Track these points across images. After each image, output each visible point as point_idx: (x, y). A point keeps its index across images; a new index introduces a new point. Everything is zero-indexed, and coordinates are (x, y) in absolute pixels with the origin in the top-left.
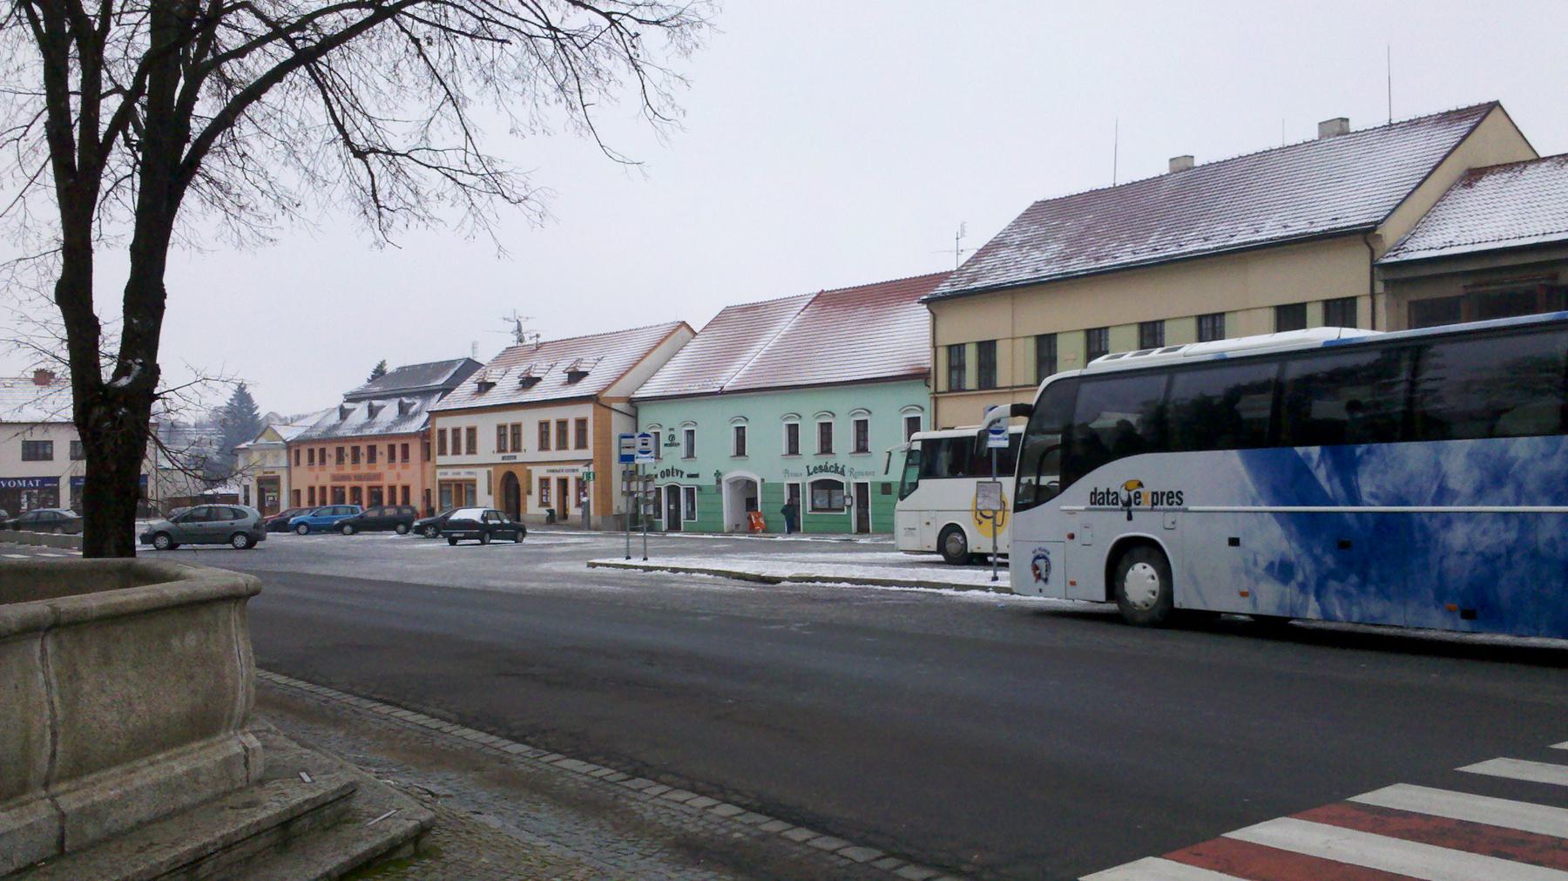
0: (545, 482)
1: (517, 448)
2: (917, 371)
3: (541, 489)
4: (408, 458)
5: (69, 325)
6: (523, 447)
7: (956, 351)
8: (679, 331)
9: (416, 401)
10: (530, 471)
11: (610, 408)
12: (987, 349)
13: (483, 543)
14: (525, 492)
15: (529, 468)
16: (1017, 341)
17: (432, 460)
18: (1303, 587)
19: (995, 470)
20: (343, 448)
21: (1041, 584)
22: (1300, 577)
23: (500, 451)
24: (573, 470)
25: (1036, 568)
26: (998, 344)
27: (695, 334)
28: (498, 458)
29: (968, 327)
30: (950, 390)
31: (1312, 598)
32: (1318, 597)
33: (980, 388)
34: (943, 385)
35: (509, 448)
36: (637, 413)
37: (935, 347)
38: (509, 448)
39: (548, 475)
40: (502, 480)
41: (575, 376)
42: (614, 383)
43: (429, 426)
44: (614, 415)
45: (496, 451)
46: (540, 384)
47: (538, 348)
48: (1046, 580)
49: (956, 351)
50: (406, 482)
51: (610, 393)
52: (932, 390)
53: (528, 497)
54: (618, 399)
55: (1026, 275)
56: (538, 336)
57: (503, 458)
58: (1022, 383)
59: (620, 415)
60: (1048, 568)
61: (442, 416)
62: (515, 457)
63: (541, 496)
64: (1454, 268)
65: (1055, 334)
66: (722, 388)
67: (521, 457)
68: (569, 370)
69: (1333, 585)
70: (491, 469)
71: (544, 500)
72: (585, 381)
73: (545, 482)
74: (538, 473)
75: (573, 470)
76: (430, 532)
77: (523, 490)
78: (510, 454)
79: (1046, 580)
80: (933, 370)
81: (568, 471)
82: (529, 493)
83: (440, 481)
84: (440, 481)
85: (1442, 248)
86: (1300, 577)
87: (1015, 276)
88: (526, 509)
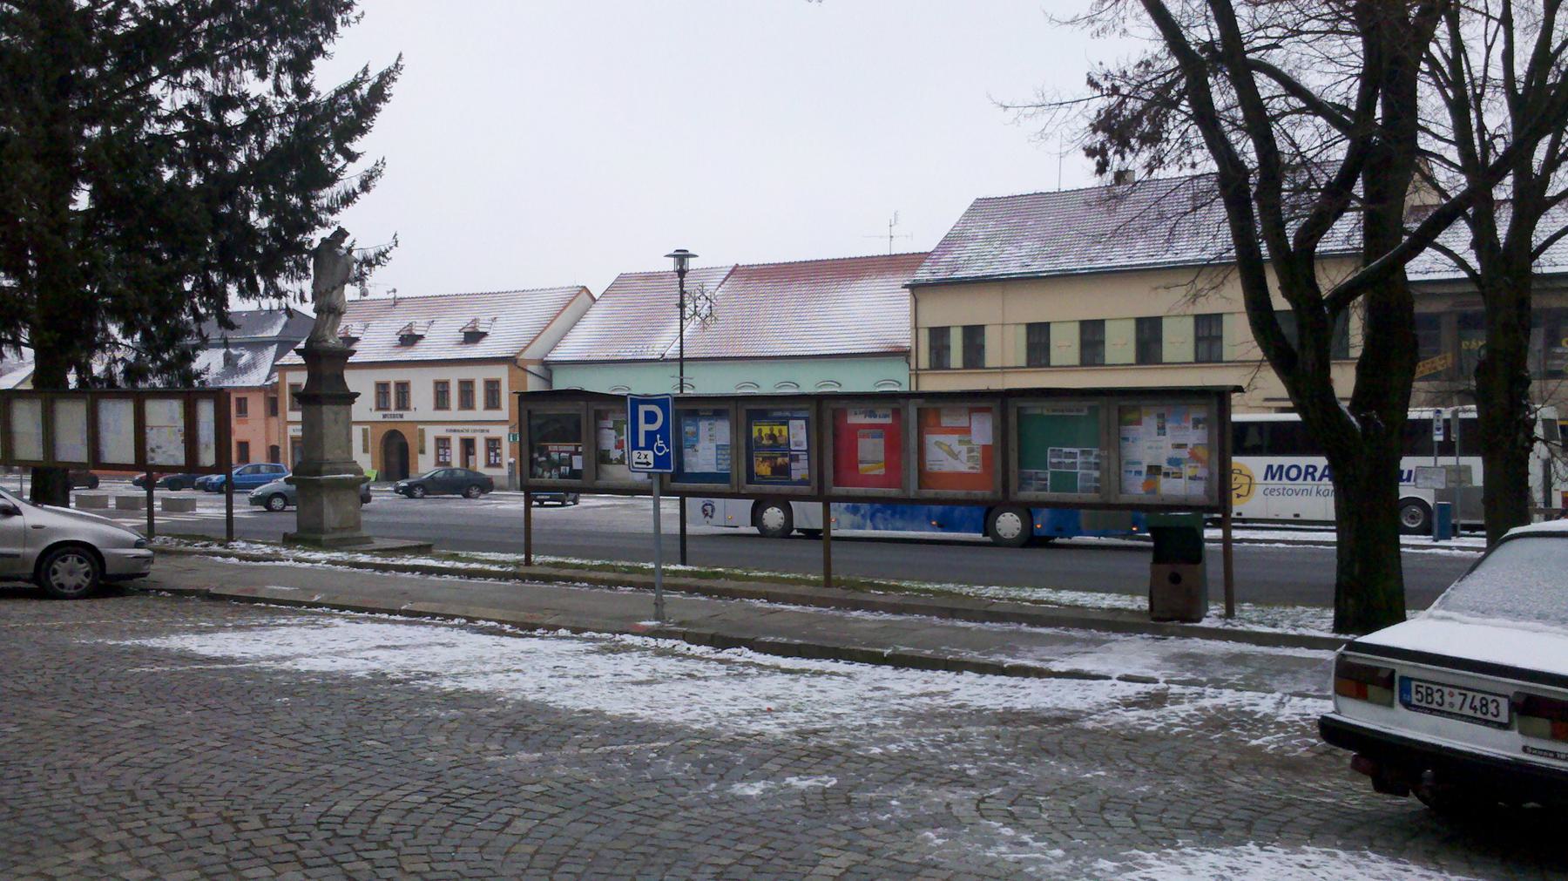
0: (442, 443)
1: (403, 404)
2: (893, 349)
3: (438, 448)
4: (246, 412)
5: (1539, 217)
6: (413, 406)
7: (939, 336)
8: (580, 296)
9: (243, 352)
10: (422, 431)
11: (526, 370)
12: (974, 335)
13: (563, 505)
14: (418, 450)
15: (420, 427)
16: (1006, 327)
17: (280, 415)
18: (863, 516)
19: (1436, 452)
20: (245, 399)
21: (708, 518)
22: (862, 512)
23: (379, 408)
24: (482, 431)
25: (704, 511)
26: (986, 328)
27: (594, 300)
28: (378, 416)
29: (954, 313)
30: (931, 368)
31: (868, 521)
32: (871, 520)
33: (965, 367)
34: (924, 361)
35: (393, 405)
36: (551, 376)
37: (916, 328)
38: (393, 405)
39: (448, 435)
40: (381, 443)
41: (473, 336)
42: (529, 345)
43: (276, 380)
44: (529, 376)
45: (374, 409)
46: (421, 342)
47: (395, 304)
48: (711, 517)
49: (939, 336)
50: (243, 438)
51: (524, 356)
52: (913, 366)
53: (420, 456)
54: (531, 362)
55: (1014, 269)
56: (395, 291)
57: (384, 416)
58: (1013, 365)
59: (534, 377)
60: (713, 510)
61: (292, 370)
62: (401, 416)
63: (438, 455)
64: (1446, 290)
65: (949, 327)
66: (663, 355)
67: (408, 416)
68: (466, 330)
69: (879, 515)
70: (368, 427)
71: (441, 459)
72: (485, 342)
73: (442, 443)
74: (432, 433)
75: (482, 431)
76: (418, 493)
77: (413, 448)
78: (393, 412)
79: (711, 517)
80: (914, 348)
81: (475, 431)
82: (422, 452)
83: (292, 438)
84: (292, 438)
85: (1427, 273)
86: (862, 512)
87: (997, 269)
88: (417, 468)
